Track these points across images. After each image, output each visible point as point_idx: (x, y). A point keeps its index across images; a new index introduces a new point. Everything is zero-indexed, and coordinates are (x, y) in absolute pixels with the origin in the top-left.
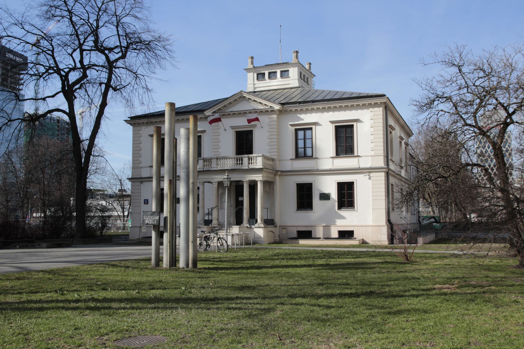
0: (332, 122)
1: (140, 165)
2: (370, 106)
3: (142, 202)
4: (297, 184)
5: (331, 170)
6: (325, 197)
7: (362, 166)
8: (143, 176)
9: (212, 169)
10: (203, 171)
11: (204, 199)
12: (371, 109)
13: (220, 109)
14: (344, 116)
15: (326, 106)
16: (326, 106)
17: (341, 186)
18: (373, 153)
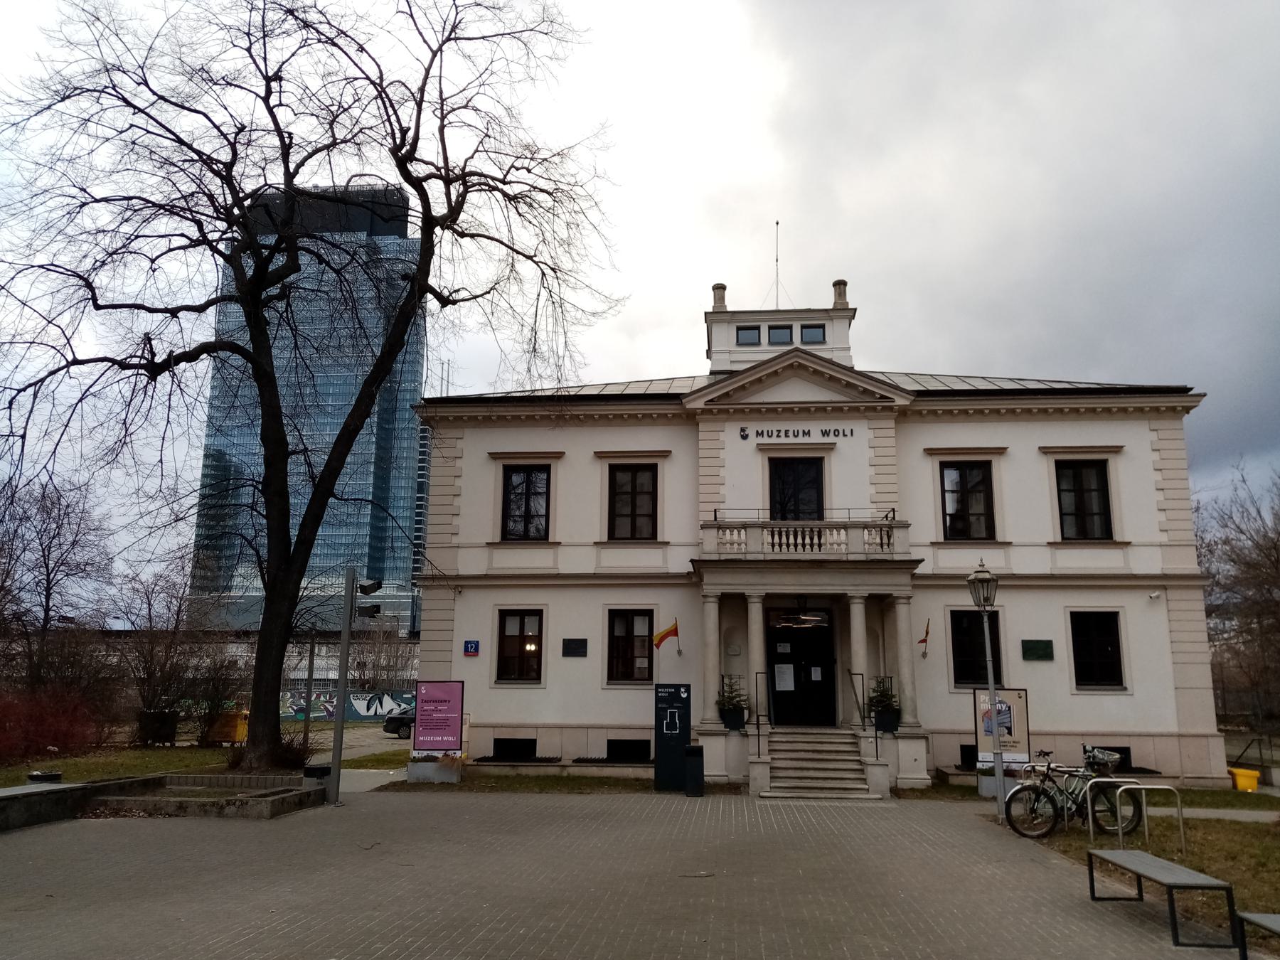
1: (455, 540)
3: (459, 648)
4: (952, 612)
5: (486, 577)
7: (564, 569)
8: (462, 572)
9: (897, 557)
10: (719, 561)
13: (727, 394)
14: (967, 436)
17: (620, 619)
18: (1164, 538)
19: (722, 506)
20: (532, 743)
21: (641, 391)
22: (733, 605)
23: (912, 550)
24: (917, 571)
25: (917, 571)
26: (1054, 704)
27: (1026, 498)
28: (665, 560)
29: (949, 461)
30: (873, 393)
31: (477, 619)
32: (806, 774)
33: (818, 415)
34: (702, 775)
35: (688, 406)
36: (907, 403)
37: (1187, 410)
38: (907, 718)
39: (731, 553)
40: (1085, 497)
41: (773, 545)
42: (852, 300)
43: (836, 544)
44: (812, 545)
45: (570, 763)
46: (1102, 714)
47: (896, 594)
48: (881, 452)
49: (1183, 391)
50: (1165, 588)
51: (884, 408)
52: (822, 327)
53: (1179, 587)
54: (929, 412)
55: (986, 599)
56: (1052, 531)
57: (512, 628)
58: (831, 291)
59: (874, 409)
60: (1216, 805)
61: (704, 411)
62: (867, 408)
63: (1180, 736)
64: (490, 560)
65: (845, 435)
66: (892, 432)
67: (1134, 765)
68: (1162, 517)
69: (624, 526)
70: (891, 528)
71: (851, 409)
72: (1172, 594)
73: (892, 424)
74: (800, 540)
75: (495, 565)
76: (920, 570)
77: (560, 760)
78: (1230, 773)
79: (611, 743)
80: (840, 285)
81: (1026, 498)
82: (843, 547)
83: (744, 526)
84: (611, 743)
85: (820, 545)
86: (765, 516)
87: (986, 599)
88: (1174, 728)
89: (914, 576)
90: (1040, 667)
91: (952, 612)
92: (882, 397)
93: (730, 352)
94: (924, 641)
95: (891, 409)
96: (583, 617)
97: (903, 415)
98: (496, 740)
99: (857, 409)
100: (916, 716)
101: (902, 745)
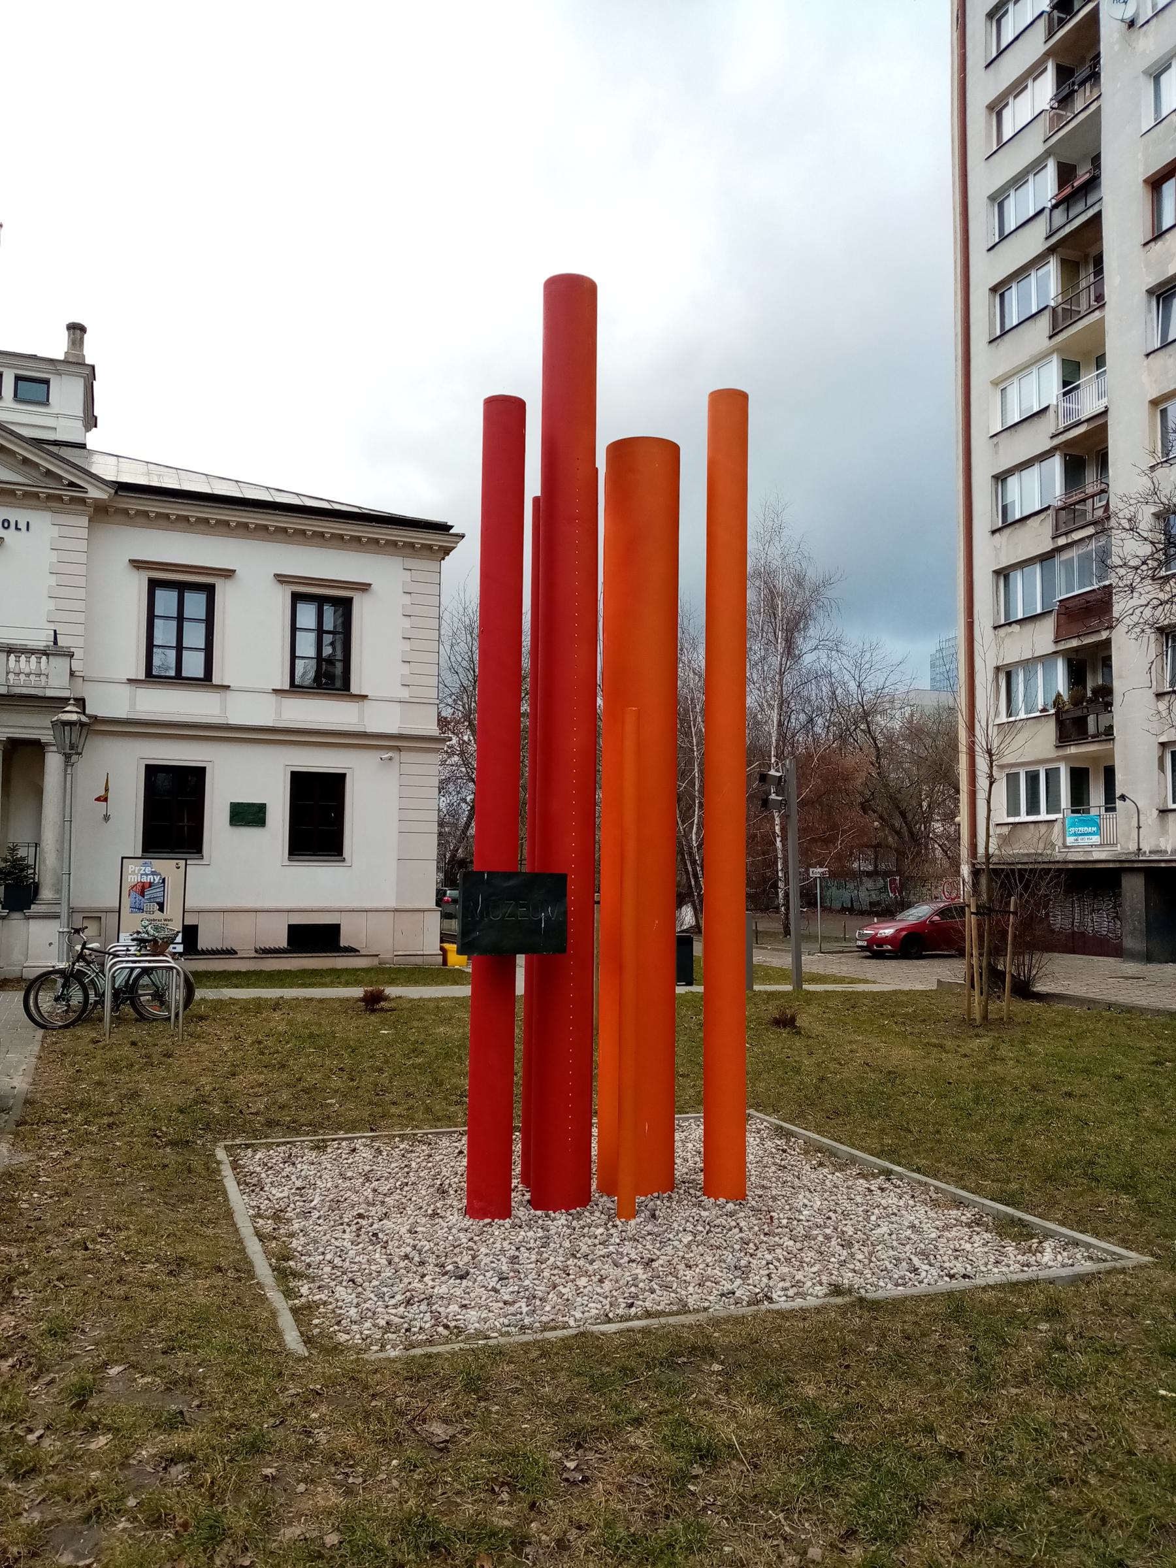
4: (293, 773)
18: (405, 694)
20: (336, 929)
26: (247, 879)
27: (255, 633)
28: (224, 708)
29: (163, 581)
30: (60, 478)
36: (104, 496)
37: (447, 551)
42: (91, 353)
47: (44, 739)
48: (66, 556)
49: (444, 528)
50: (399, 749)
51: (73, 500)
52: (46, 382)
53: (410, 749)
54: (138, 513)
58: (64, 335)
59: (59, 498)
62: (49, 497)
63: (396, 910)
64: (279, 713)
65: (17, 529)
66: (84, 533)
68: (406, 669)
71: (26, 494)
72: (406, 756)
73: (85, 521)
75: (138, 708)
78: (442, 949)
79: (292, 929)
80: (77, 330)
81: (255, 633)
84: (292, 929)
88: (392, 904)
91: (293, 773)
92: (72, 484)
94: (105, 799)
95: (83, 501)
97: (101, 513)
98: (290, 926)
99: (36, 495)
101: (35, 926)
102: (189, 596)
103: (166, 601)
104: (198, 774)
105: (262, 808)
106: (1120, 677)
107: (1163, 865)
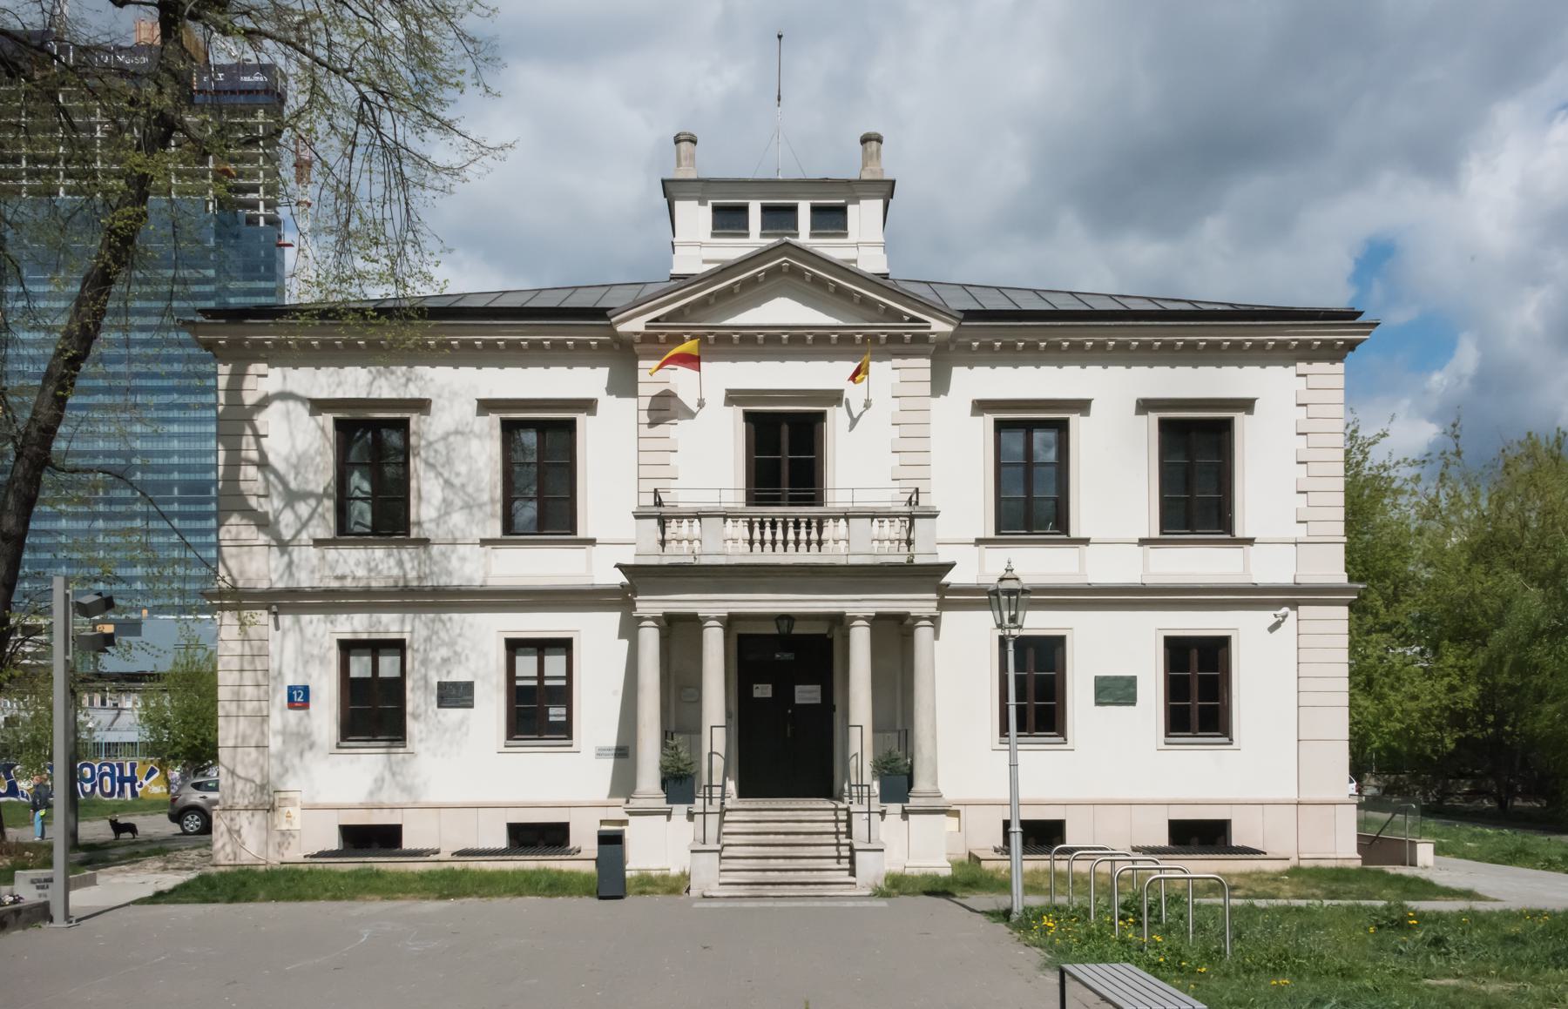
0: (1145, 406)
2: (1308, 353)
6: (455, 695)
11: (934, 737)
12: (1302, 367)
15: (547, 339)
16: (269, 339)
17: (1178, 650)
18: (1300, 532)
19: (673, 484)
21: (554, 304)
22: (680, 634)
23: (939, 549)
24: (945, 580)
25: (945, 580)
27: (1114, 473)
31: (308, 651)
32: (773, 863)
33: (768, 348)
34: (623, 870)
35: (621, 328)
36: (949, 329)
38: (921, 784)
39: (677, 554)
40: (1197, 473)
41: (751, 542)
43: (845, 544)
44: (797, 543)
45: (449, 857)
46: (1198, 778)
47: (914, 612)
55: (1013, 619)
56: (1147, 519)
57: (360, 667)
60: (504, 874)
61: (646, 338)
67: (1234, 844)
69: (527, 512)
70: (912, 518)
71: (841, 339)
74: (780, 536)
76: (951, 578)
77: (437, 852)
81: (1114, 473)
82: (842, 544)
83: (699, 516)
85: (820, 543)
86: (735, 497)
87: (1013, 619)
89: (944, 590)
90: (1116, 713)
92: (914, 319)
93: (701, 245)
95: (923, 339)
96: (476, 647)
100: (935, 783)
102: (1039, 436)
103: (1015, 442)
104: (1059, 642)
105: (1131, 682)
106: (416, 717)
107: (850, 904)
